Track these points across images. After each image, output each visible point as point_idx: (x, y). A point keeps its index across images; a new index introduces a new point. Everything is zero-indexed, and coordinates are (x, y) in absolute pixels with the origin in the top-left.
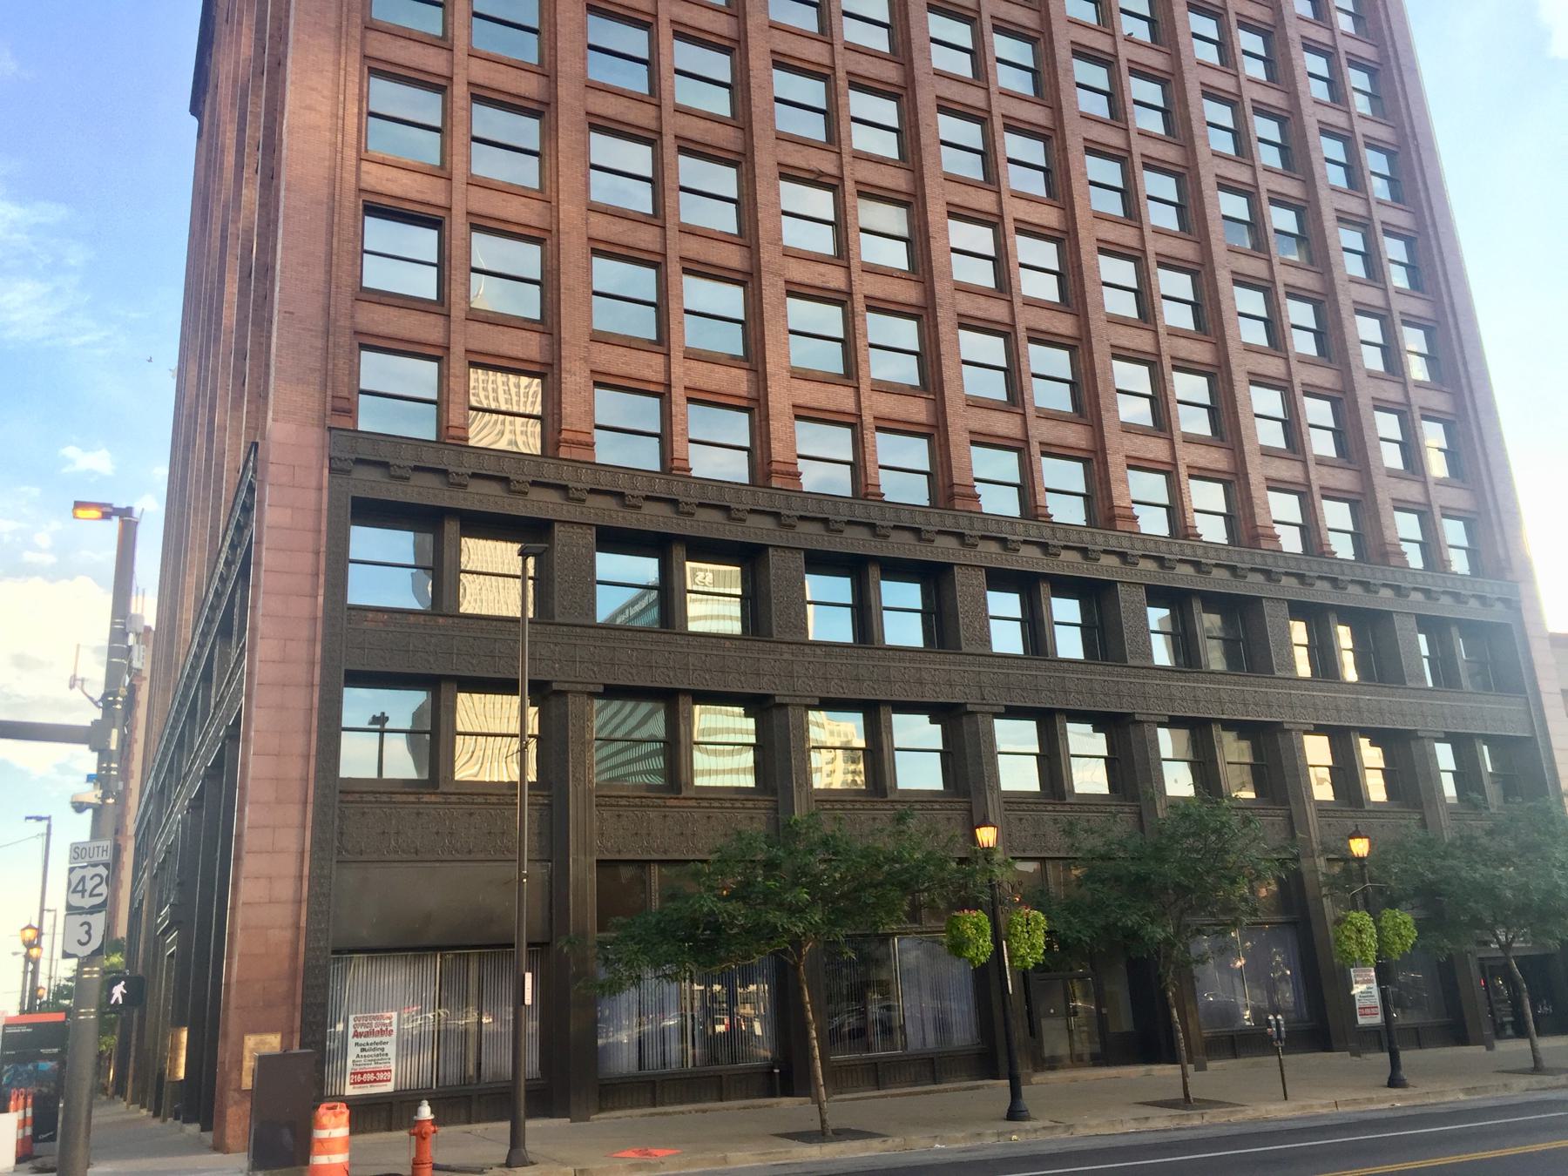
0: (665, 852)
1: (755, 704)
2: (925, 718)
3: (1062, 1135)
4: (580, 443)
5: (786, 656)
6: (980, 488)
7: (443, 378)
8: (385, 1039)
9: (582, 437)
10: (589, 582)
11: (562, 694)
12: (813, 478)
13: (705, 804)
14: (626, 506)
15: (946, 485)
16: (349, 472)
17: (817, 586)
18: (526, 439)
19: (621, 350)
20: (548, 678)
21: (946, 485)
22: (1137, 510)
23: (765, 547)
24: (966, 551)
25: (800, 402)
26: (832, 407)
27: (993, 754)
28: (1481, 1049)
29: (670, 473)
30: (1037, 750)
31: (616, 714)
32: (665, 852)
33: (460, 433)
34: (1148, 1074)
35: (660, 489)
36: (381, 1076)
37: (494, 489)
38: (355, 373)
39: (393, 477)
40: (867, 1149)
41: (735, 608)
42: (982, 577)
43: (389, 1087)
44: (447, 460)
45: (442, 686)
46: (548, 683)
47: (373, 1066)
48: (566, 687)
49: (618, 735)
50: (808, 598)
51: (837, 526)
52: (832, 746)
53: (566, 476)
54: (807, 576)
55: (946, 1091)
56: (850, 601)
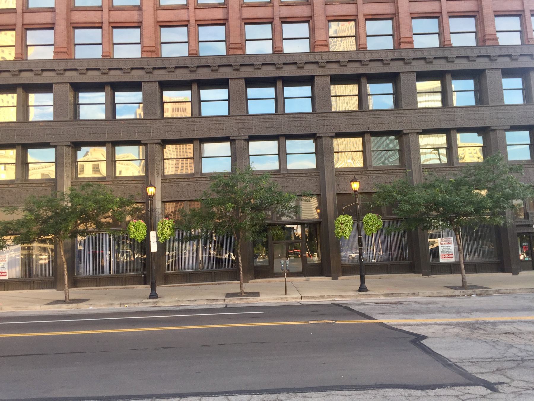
0: (345, 191)
1: (482, 131)
2: (476, 134)
3: (285, 301)
4: (407, 42)
5: (148, 125)
6: (498, 35)
7: (357, 27)
8: (450, 245)
9: (408, 40)
10: (414, 93)
11: (320, 137)
12: (504, 40)
13: (377, 172)
14: (449, 62)
15: (484, 38)
16: (238, 69)
17: (507, 83)
18: (388, 44)
19: (83, 12)
20: (402, 129)
21: (484, 38)
22: (498, 35)
23: (228, 79)
24: (235, 72)
25: (495, 10)
26: (177, 19)
27: (505, 146)
28: (509, 275)
29: (444, 47)
30: (529, 142)
31: (378, 142)
32: (172, 198)
33: (280, 49)
34: (307, 280)
35: (440, 54)
36: (3, 274)
37: (464, 61)
38: (411, 28)
39: (298, 67)
40: (60, 308)
41: (520, 93)
42: (500, 73)
43: (6, 278)
44: (361, 57)
45: (23, 148)
46: (402, 131)
47: (447, 253)
48: (408, 131)
49: (381, 149)
50: (454, 90)
51: (473, 59)
52: (430, 149)
53: (404, 55)
54: (453, 82)
55: (209, 284)
56: (521, 87)
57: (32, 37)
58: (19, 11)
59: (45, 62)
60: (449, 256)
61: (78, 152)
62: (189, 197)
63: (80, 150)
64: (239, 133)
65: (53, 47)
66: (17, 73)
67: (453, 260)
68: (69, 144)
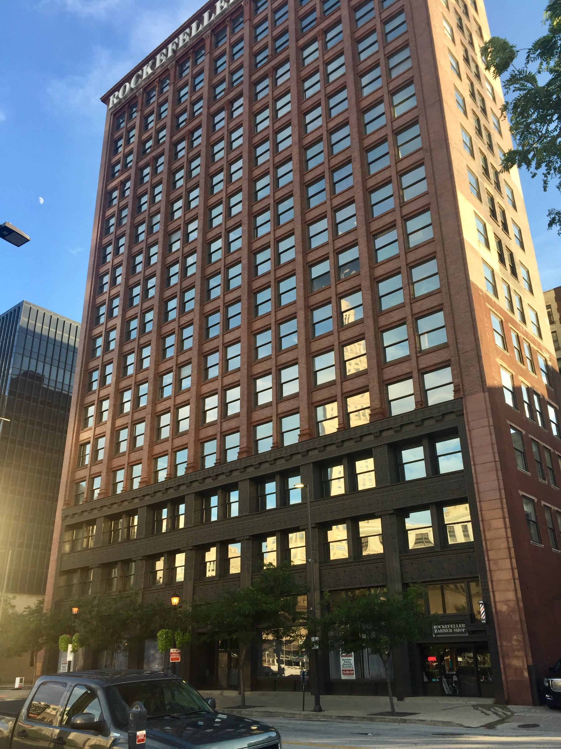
57: (430, 379)
58: (414, 356)
59: (292, 447)
60: (349, 672)
61: (406, 520)
62: (432, 577)
63: (409, 517)
64: (394, 501)
65: (452, 385)
66: (399, 429)
67: (354, 677)
68: (392, 512)
